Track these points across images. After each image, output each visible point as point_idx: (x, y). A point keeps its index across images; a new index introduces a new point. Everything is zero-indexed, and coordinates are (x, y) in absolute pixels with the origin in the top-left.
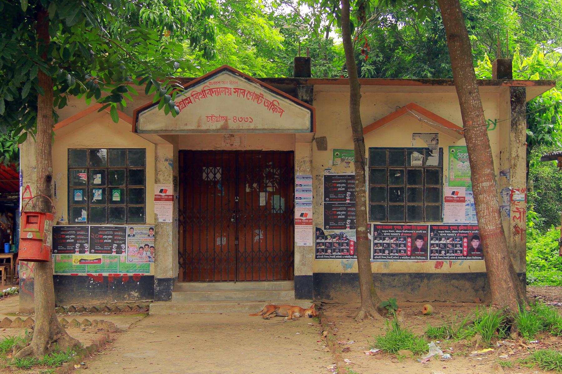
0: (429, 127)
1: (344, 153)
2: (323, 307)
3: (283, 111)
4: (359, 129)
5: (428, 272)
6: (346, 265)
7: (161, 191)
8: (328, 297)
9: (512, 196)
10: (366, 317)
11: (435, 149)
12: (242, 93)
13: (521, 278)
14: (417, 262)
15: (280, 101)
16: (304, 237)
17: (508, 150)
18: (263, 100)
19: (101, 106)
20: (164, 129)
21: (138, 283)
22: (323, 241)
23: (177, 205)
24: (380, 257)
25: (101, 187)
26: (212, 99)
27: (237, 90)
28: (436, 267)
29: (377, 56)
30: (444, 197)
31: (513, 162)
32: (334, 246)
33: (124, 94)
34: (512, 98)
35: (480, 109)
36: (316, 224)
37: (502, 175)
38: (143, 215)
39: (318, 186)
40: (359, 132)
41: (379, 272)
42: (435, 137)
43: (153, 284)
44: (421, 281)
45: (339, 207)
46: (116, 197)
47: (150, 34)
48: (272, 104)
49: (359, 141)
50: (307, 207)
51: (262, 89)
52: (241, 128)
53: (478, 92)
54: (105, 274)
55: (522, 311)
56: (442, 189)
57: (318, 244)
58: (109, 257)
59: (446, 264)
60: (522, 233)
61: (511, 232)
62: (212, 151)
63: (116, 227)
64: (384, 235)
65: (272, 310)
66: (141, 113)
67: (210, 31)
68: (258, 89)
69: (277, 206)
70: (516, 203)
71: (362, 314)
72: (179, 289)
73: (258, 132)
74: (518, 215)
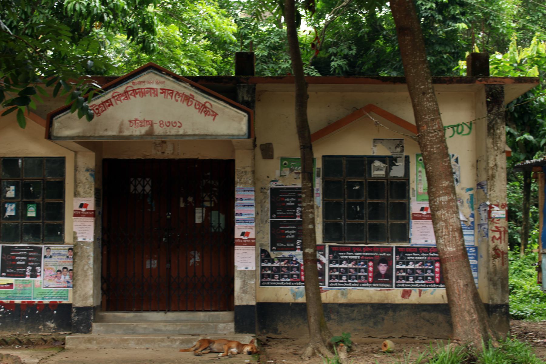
0: (387, 131)
1: (294, 162)
2: (269, 343)
3: (216, 114)
4: (306, 135)
5: (393, 302)
6: (296, 293)
7: (82, 206)
8: (275, 331)
9: (490, 212)
10: (314, 354)
11: (400, 157)
12: (170, 93)
13: (503, 310)
14: (381, 290)
15: (213, 103)
16: (245, 260)
17: (485, 158)
18: (194, 102)
19: (6, 108)
20: (81, 135)
21: (55, 312)
22: (269, 264)
23: (100, 222)
24: (336, 284)
25: (13, 201)
26: (136, 101)
27: (164, 91)
28: (403, 296)
29: (350, 49)
30: (411, 213)
31: (490, 172)
32: (282, 271)
33: (31, 97)
34: (487, 98)
35: (437, 112)
36: (261, 245)
37: (479, 187)
38: (61, 233)
39: (264, 201)
40: (307, 139)
41: (336, 302)
42: (400, 144)
43: (71, 312)
44: (386, 313)
45: (287, 225)
46: (32, 212)
47: (61, 30)
48: (204, 106)
49: (307, 148)
50: (249, 225)
51: (193, 89)
52: (168, 133)
53: (433, 92)
54: (18, 301)
55: (487, 348)
56: (409, 204)
57: (263, 268)
58: (23, 282)
59: (415, 293)
60: (503, 257)
61: (490, 255)
62: (140, 159)
63: (31, 248)
64: (340, 259)
65: (206, 345)
66: (54, 118)
67: (149, 21)
68: (187, 90)
69: (215, 224)
70: (495, 220)
71: (309, 350)
72: (100, 320)
73: (187, 138)
74: (497, 235)
